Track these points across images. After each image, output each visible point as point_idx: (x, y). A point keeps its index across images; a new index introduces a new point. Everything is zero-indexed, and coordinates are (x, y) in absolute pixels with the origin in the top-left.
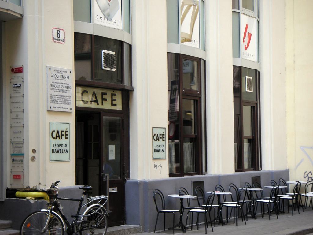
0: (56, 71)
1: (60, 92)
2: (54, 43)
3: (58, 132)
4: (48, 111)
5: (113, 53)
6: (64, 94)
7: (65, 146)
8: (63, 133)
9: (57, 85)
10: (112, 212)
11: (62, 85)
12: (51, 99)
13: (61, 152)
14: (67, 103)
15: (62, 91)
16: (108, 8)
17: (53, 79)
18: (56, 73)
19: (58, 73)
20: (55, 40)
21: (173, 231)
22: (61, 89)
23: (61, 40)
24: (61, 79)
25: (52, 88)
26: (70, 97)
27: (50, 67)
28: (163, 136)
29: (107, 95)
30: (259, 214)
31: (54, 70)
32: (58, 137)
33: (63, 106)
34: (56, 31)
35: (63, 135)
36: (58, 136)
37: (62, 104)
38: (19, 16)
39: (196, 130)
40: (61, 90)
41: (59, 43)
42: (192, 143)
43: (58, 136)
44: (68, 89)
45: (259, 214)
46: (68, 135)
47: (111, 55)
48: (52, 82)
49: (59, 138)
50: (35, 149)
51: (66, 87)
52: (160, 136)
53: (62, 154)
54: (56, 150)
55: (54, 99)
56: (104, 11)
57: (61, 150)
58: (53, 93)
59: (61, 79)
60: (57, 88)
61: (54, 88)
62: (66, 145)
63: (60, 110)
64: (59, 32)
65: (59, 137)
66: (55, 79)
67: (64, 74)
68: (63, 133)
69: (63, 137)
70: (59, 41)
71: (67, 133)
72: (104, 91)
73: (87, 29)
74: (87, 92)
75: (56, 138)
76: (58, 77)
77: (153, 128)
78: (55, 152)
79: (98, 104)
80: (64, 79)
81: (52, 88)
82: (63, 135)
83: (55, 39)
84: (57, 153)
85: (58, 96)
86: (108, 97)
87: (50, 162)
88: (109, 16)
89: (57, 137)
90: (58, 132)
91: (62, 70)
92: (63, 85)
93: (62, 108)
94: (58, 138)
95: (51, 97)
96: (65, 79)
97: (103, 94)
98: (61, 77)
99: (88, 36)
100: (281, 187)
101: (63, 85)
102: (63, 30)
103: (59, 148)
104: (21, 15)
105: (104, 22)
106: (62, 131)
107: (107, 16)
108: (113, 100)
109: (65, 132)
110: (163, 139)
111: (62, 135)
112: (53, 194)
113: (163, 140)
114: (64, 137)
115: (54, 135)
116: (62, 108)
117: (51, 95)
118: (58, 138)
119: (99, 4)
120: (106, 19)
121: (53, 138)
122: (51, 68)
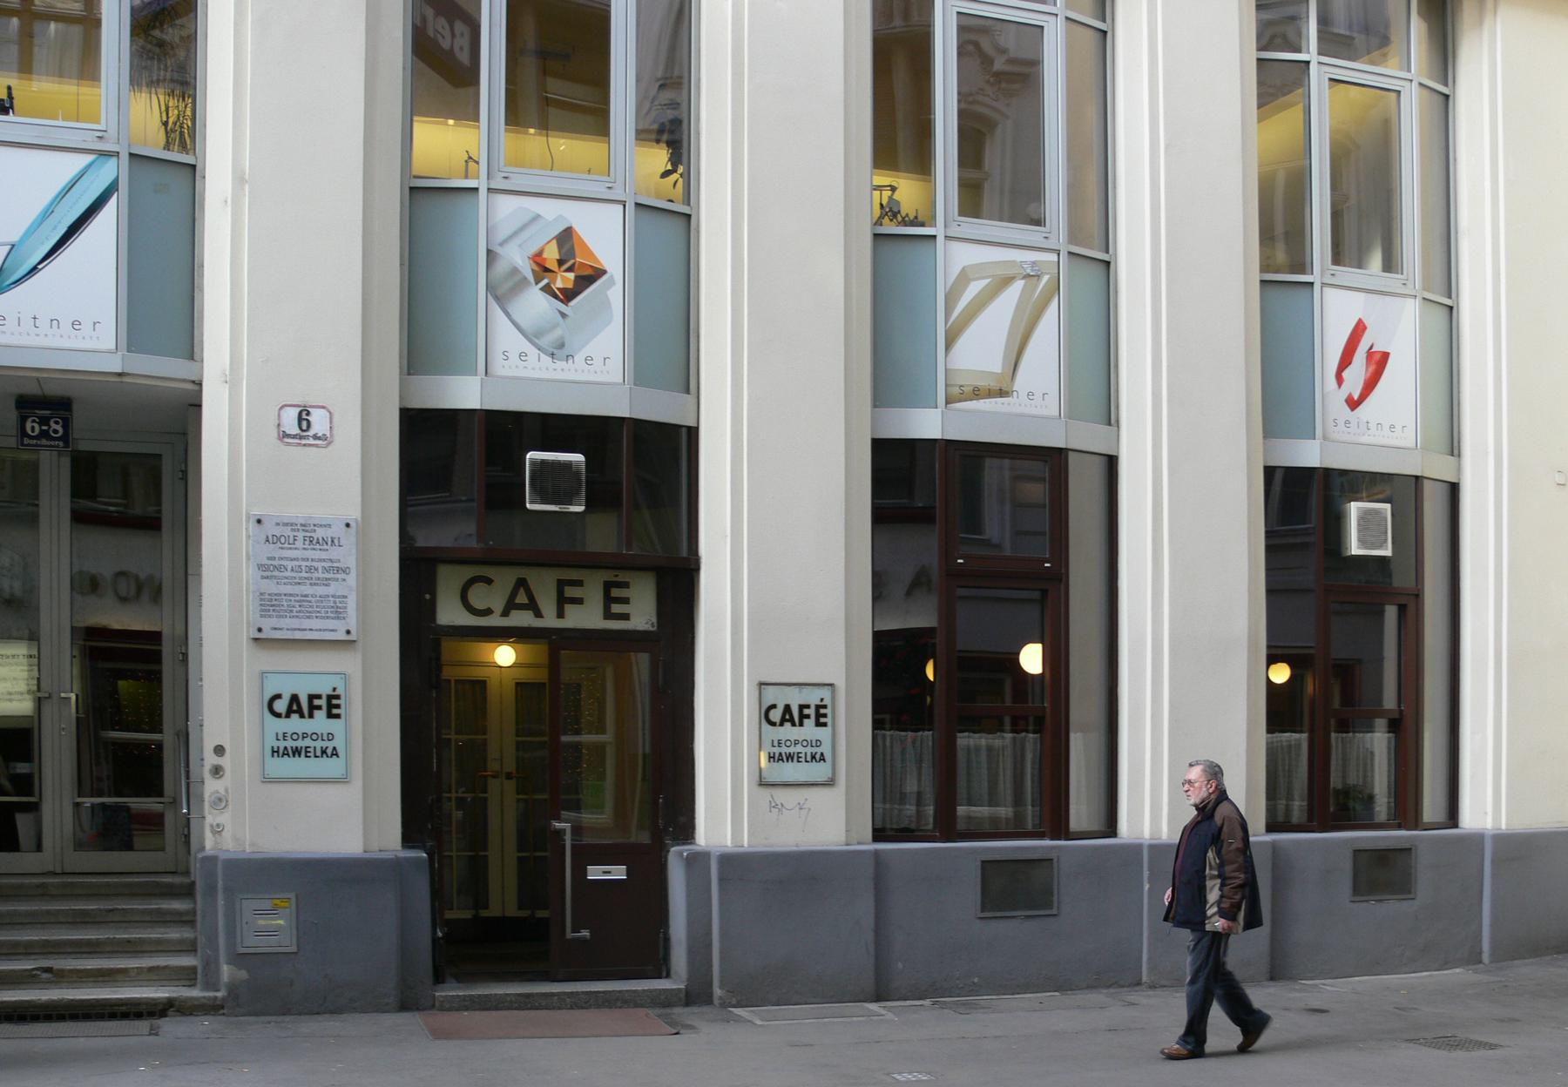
0: (286, 524)
1: (299, 583)
2: (283, 447)
4: (256, 640)
5: (578, 458)
6: (321, 590)
7: (814, 745)
9: (289, 564)
10: (588, 937)
11: (308, 564)
12: (261, 605)
13: (800, 760)
14: (329, 614)
15: (308, 582)
16: (555, 326)
17: (271, 550)
18: (278, 531)
19: (293, 530)
20: (286, 440)
22: (304, 574)
23: (316, 437)
24: (304, 549)
25: (265, 574)
26: (346, 597)
27: (259, 517)
29: (582, 586)
31: (278, 524)
33: (307, 624)
34: (292, 414)
35: (808, 717)
36: (295, 708)
37: (308, 617)
38: (190, 387)
39: (1063, 694)
40: (306, 578)
41: (305, 445)
42: (1038, 735)
44: (338, 576)
47: (567, 466)
48: (269, 558)
50: (221, 746)
51: (326, 570)
53: (313, 759)
54: (784, 755)
55: (272, 606)
56: (535, 337)
57: (800, 755)
58: (271, 587)
59: (304, 549)
60: (288, 574)
61: (276, 573)
63: (298, 635)
64: (308, 414)
66: (282, 548)
67: (320, 533)
69: (317, 713)
70: (304, 442)
72: (573, 575)
73: (1308, 454)
74: (489, 581)
76: (291, 542)
77: (761, 684)
78: (779, 760)
79: (538, 614)
80: (318, 547)
81: (265, 574)
82: (808, 717)
83: (289, 436)
84: (292, 758)
85: (291, 595)
86: (593, 593)
87: (263, 782)
88: (562, 346)
91: (311, 522)
92: (315, 564)
93: (311, 630)
95: (261, 600)
96: (325, 547)
97: (561, 584)
98: (307, 542)
99: (684, 430)
101: (315, 564)
102: (323, 407)
103: (300, 743)
104: (193, 382)
105: (539, 367)
107: (551, 350)
108: (609, 600)
109: (324, 698)
114: (810, 723)
116: (311, 630)
117: (261, 594)
118: (788, 725)
119: (515, 317)
120: (546, 359)
122: (262, 519)
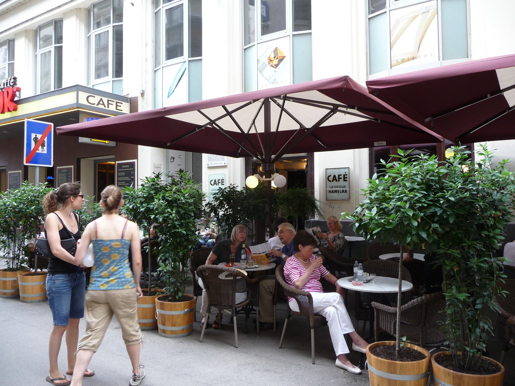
3: (215, 181)
8: (219, 181)
21: (209, 322)
28: (222, 181)
30: (261, 249)
32: (335, 180)
35: (220, 183)
36: (335, 179)
43: (335, 179)
45: (261, 249)
46: (223, 182)
49: (217, 185)
52: (218, 181)
62: (345, 187)
65: (216, 184)
68: (219, 181)
71: (223, 181)
75: (214, 185)
82: (220, 183)
89: (214, 184)
90: (215, 181)
94: (215, 185)
100: (280, 215)
106: (218, 180)
110: (222, 183)
111: (219, 183)
112: (357, 266)
113: (344, 180)
115: (212, 182)
118: (215, 185)
121: (212, 185)
